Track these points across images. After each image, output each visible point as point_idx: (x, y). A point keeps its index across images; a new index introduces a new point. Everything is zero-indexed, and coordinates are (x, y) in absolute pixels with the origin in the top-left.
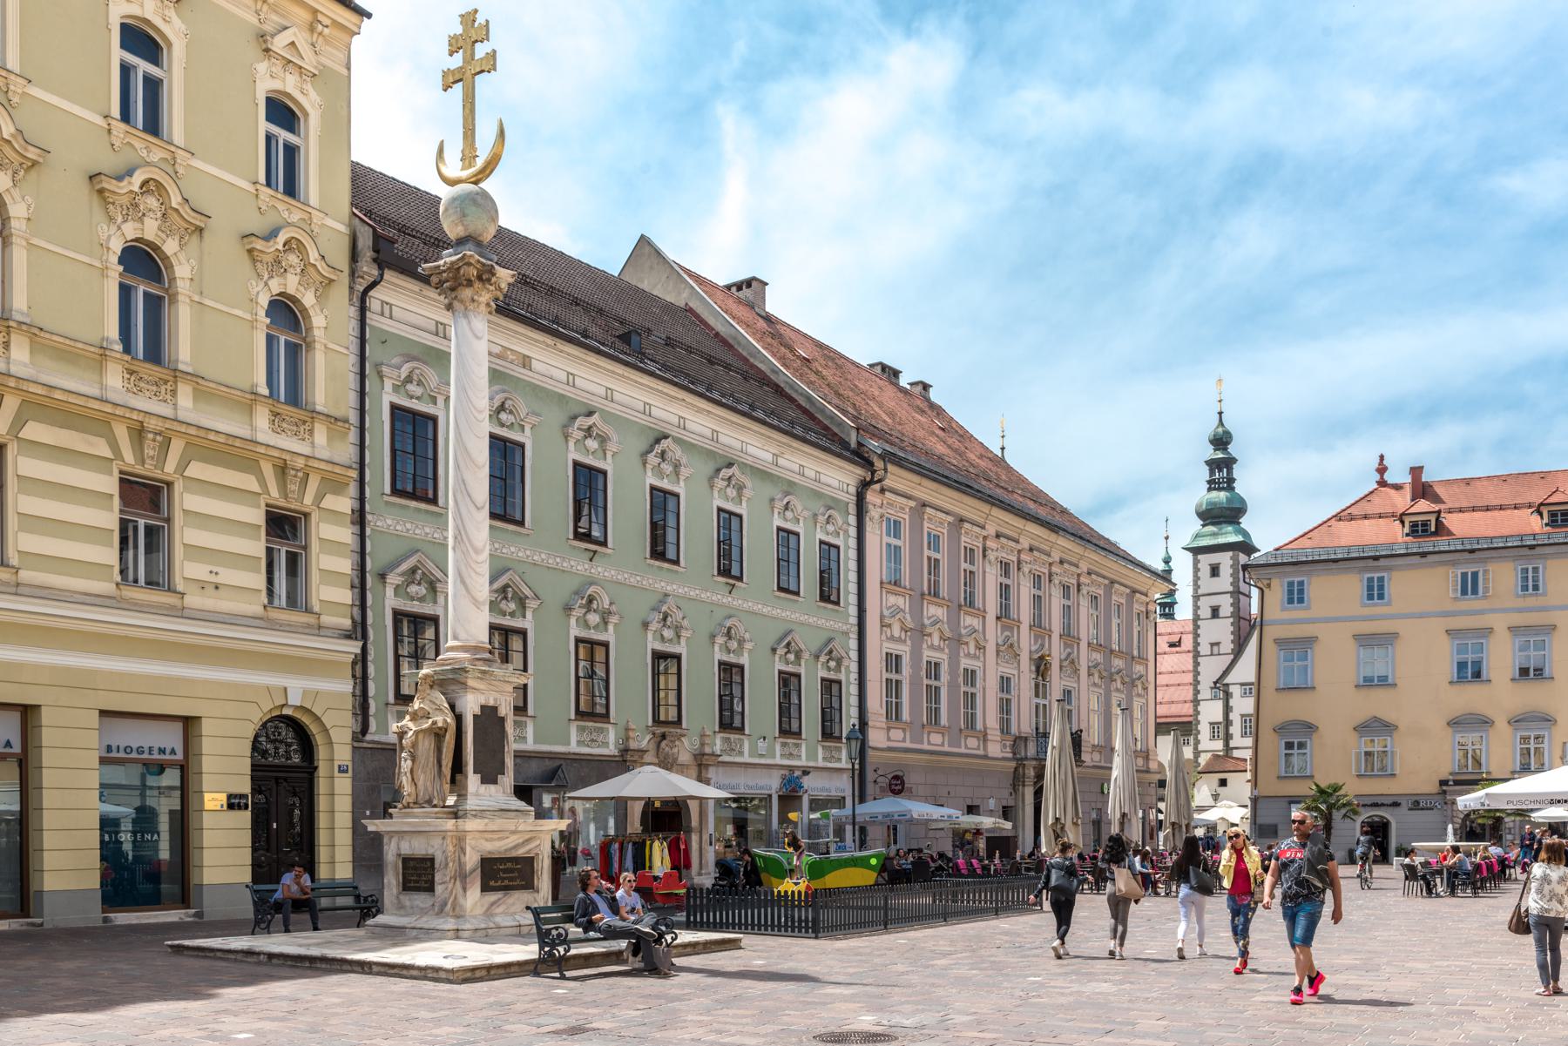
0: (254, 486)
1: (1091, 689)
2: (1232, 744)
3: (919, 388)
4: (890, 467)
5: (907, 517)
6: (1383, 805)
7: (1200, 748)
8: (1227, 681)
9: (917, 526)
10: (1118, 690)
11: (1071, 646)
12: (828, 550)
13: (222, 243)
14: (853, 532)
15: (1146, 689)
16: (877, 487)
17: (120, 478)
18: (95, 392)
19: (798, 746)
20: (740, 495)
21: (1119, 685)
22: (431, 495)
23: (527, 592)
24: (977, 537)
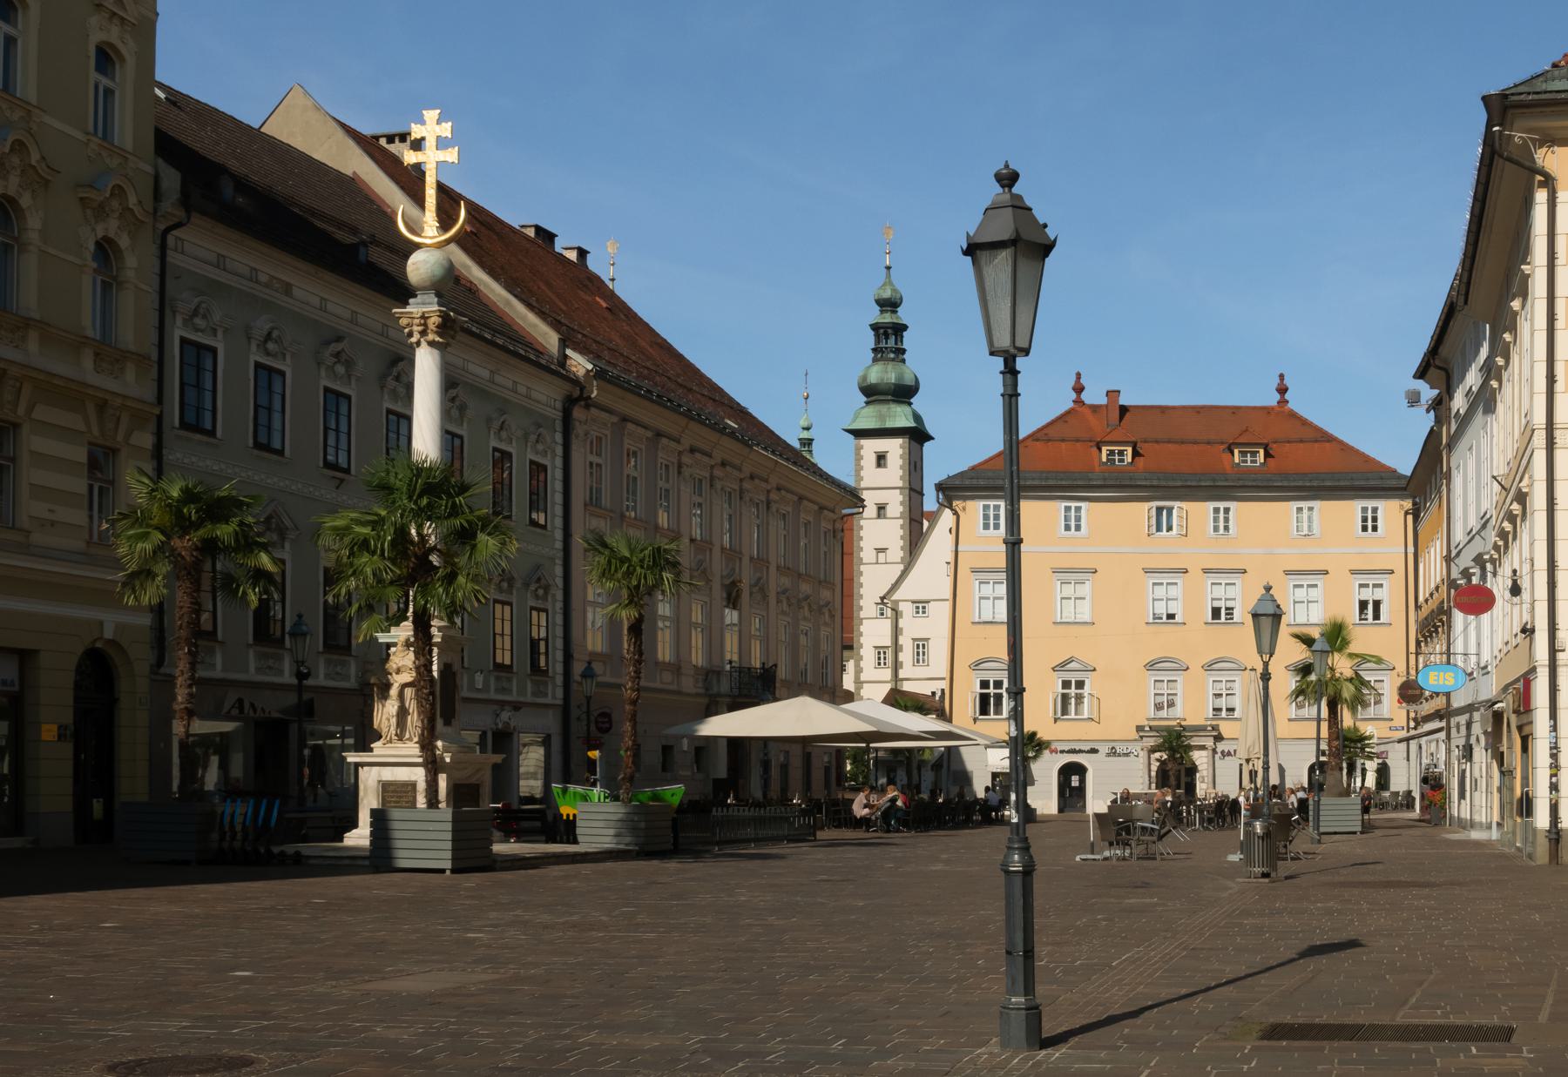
0: (82, 428)
1: (780, 617)
2: (902, 674)
6: (1080, 751)
7: (863, 677)
8: (895, 597)
10: (805, 619)
12: (538, 469)
14: (559, 450)
15: (832, 616)
19: (509, 680)
20: (462, 416)
21: (807, 613)
22: (208, 426)
23: (288, 523)
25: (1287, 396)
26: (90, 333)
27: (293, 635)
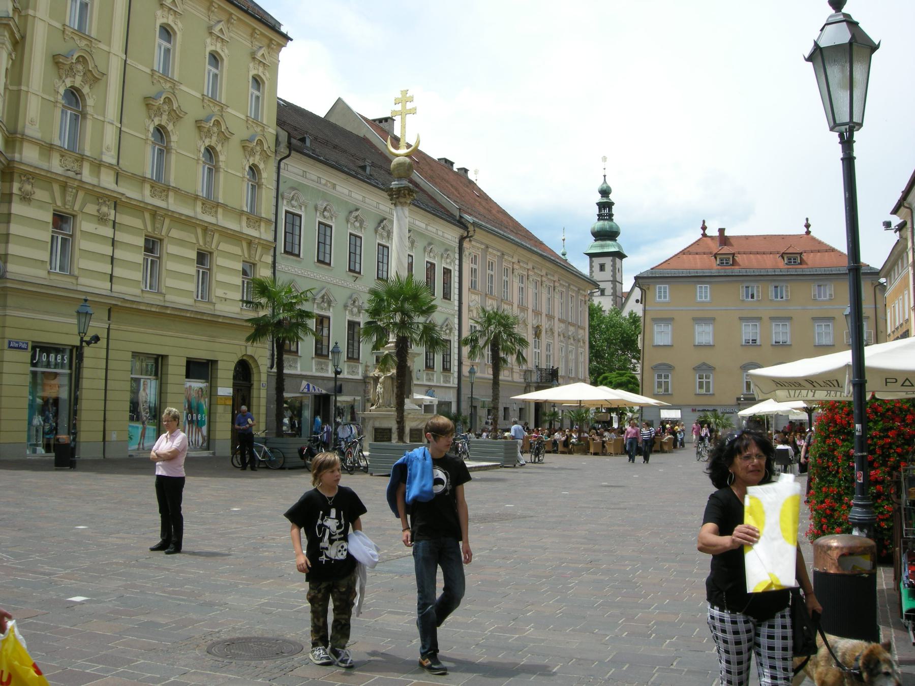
0: (240, 253)
3: (463, 171)
4: (476, 229)
5: (480, 253)
9: (484, 258)
10: (572, 344)
11: (550, 320)
12: (447, 272)
13: (188, 122)
14: (457, 262)
16: (468, 239)
17: (54, 214)
18: (45, 167)
19: (433, 375)
24: (495, 256)
25: (810, 229)
26: (245, 209)
27: (333, 352)
